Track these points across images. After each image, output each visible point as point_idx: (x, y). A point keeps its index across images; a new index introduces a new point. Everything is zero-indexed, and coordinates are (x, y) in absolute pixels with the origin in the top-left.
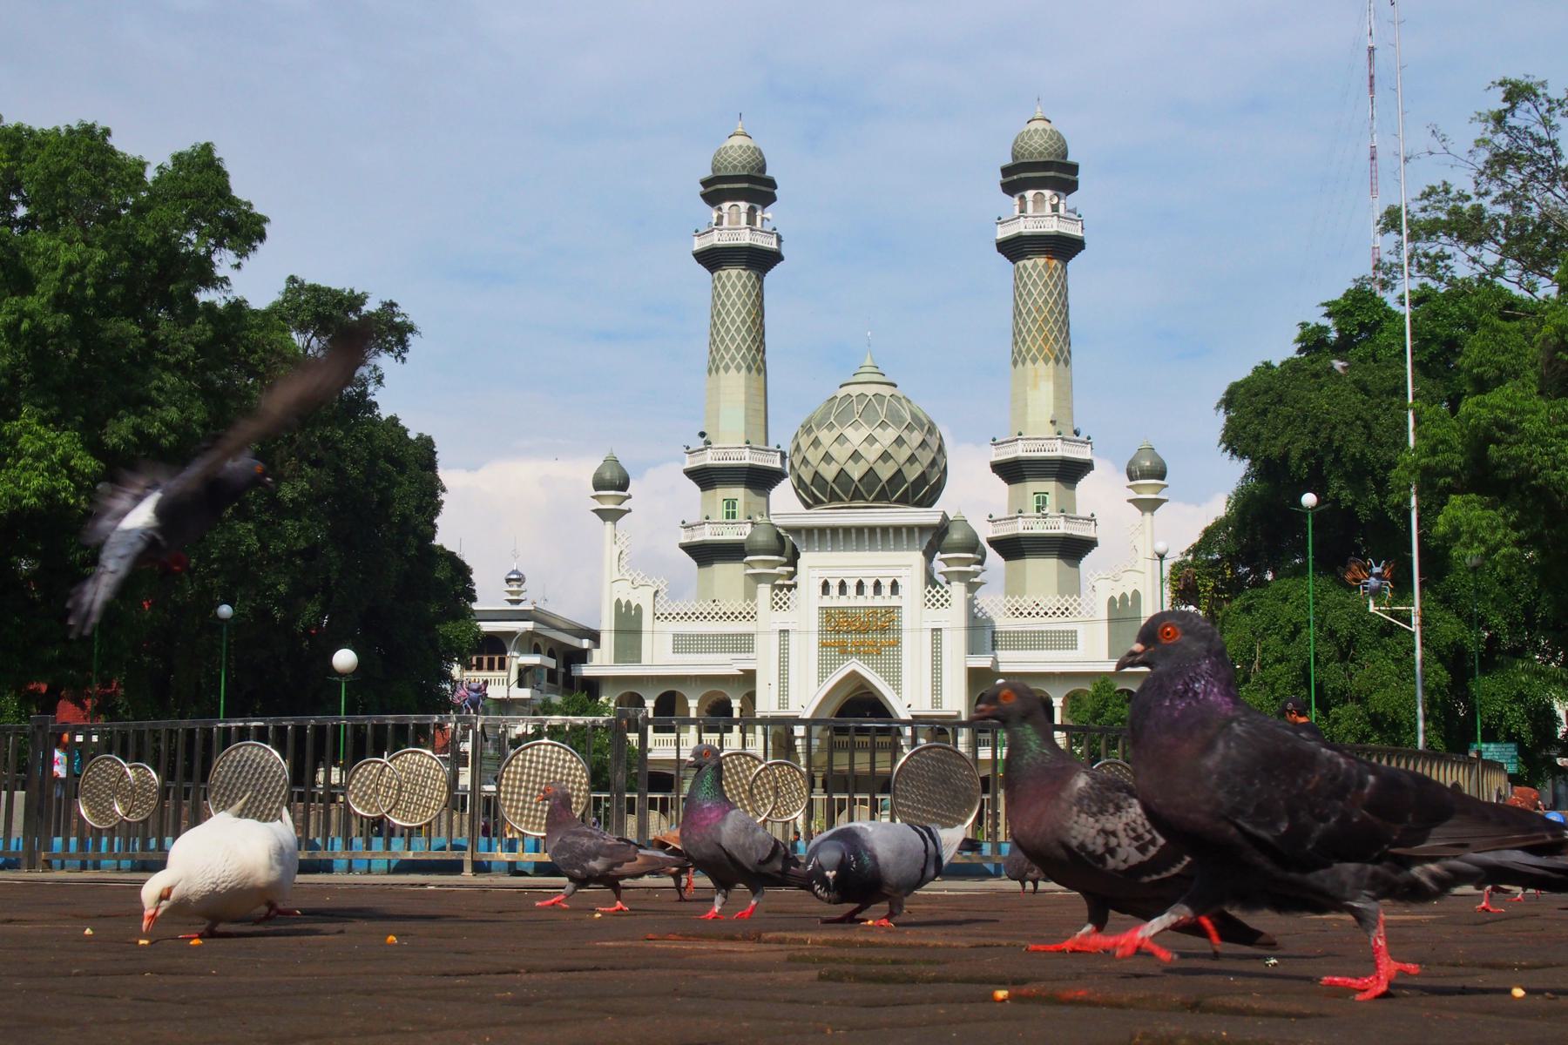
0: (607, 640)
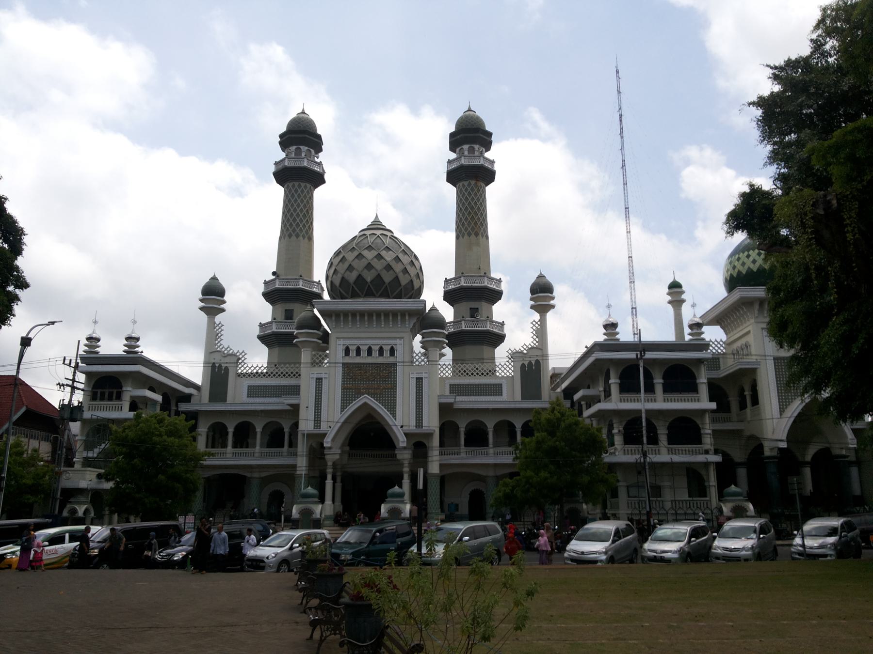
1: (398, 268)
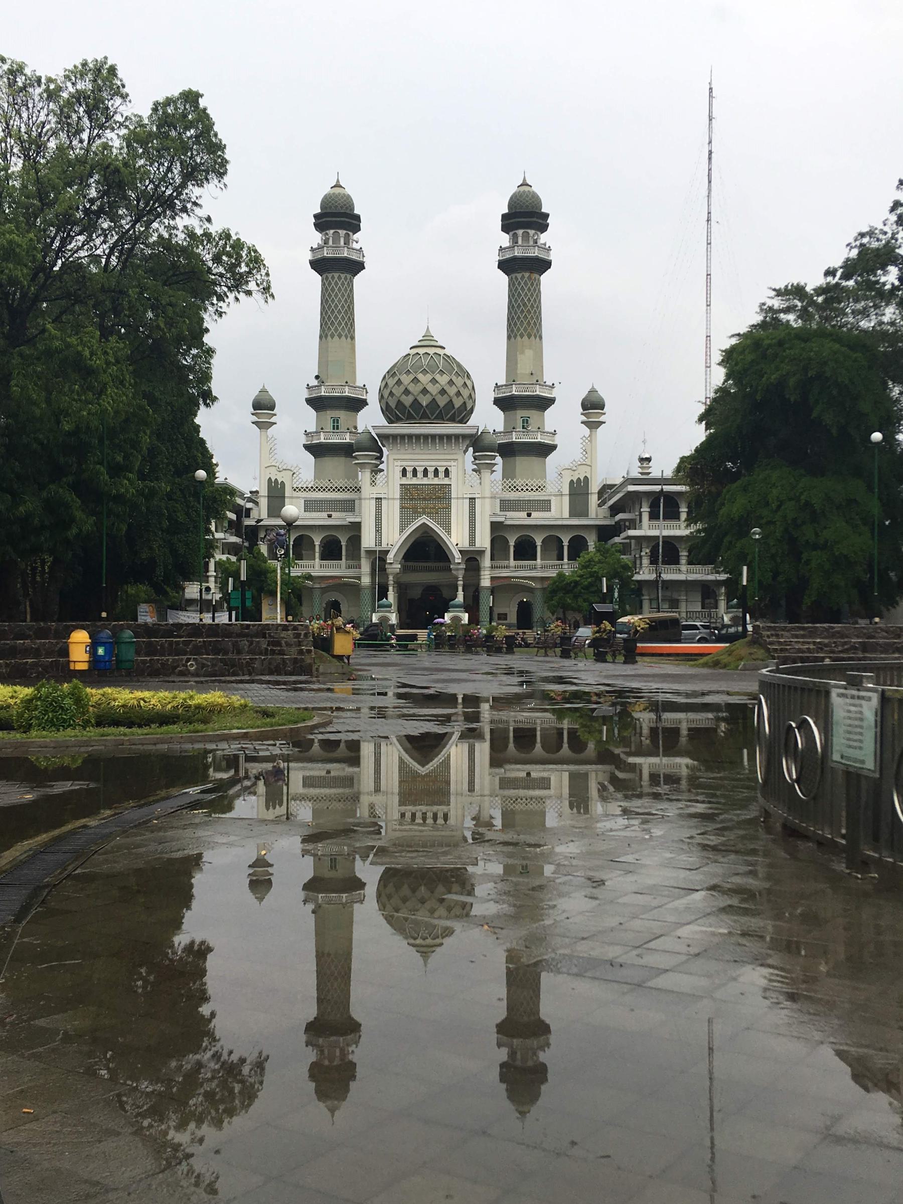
0: (264, 502)
1: (452, 391)
